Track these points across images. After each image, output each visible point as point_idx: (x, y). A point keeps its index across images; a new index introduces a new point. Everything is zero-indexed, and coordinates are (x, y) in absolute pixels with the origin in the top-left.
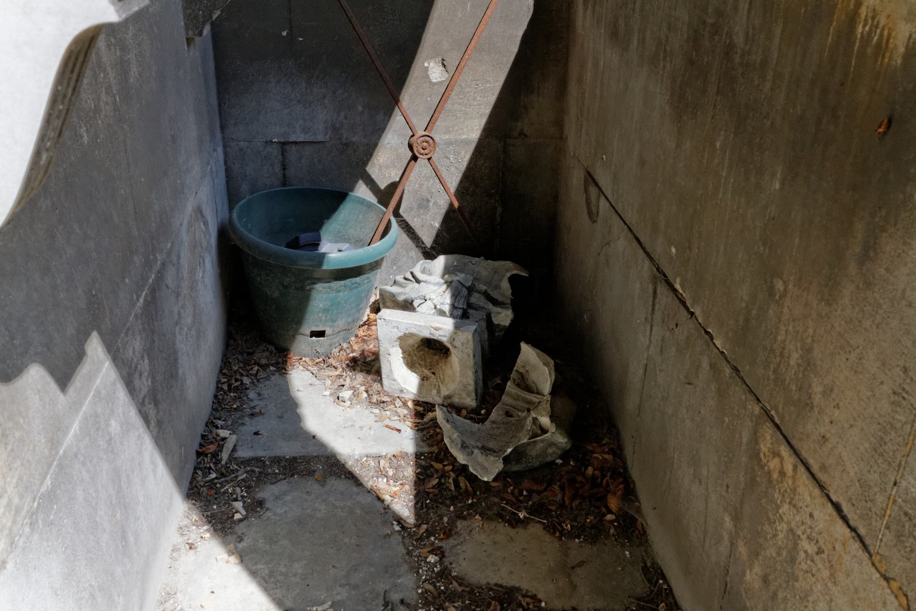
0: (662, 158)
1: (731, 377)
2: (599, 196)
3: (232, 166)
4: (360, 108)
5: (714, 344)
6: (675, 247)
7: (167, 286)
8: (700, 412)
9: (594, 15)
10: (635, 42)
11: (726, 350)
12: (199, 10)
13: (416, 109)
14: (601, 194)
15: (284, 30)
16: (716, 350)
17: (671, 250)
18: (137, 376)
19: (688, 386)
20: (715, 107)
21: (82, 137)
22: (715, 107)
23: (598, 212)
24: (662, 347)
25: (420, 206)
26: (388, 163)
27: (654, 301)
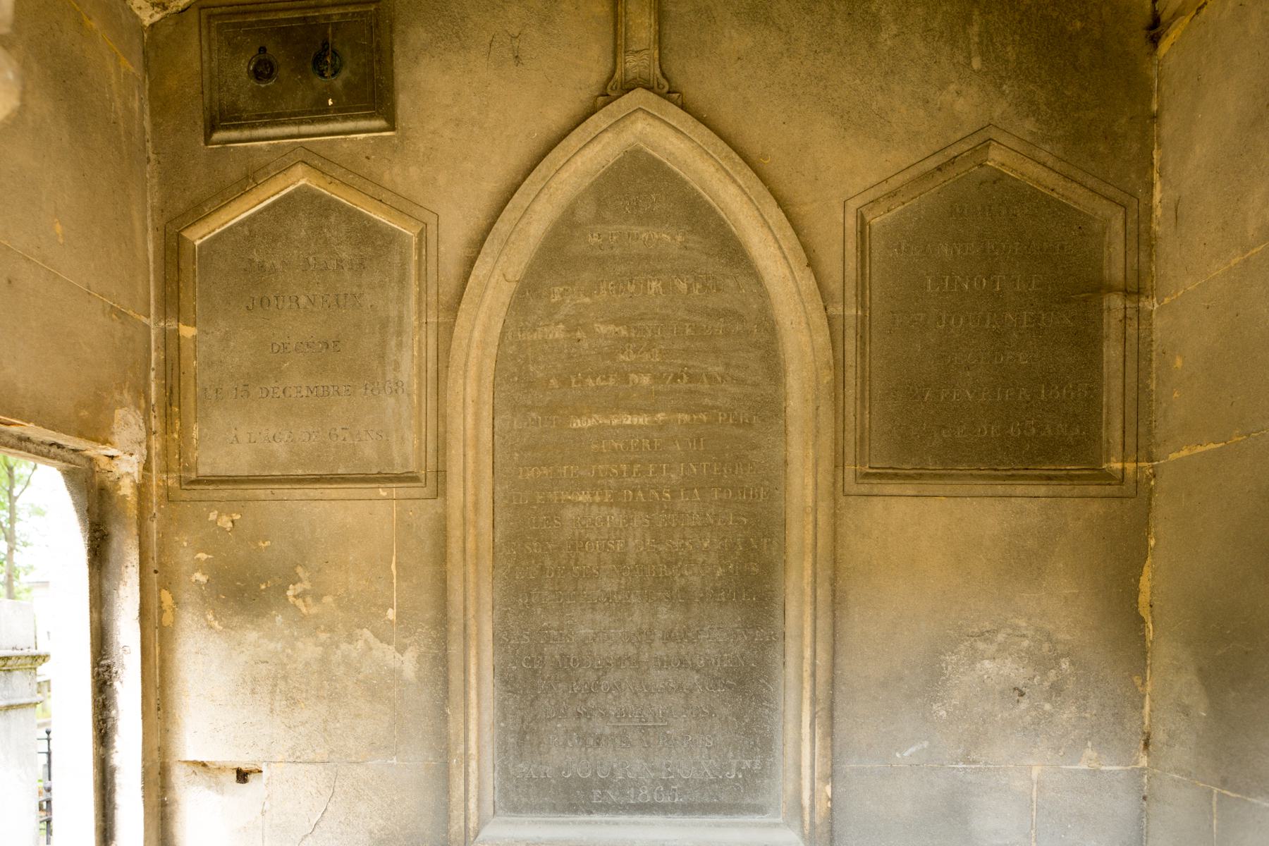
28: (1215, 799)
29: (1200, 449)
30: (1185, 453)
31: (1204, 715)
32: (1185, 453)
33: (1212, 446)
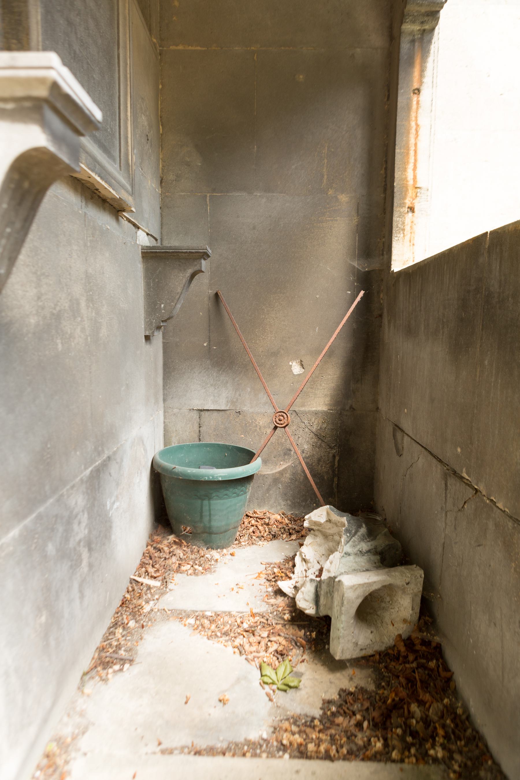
0: (446, 390)
1: (514, 528)
2: (403, 436)
3: (168, 424)
4: (249, 389)
5: (498, 507)
6: (460, 447)
7: (110, 474)
8: (490, 566)
9: (395, 327)
10: (423, 328)
11: (507, 508)
12: (153, 319)
13: (284, 390)
14: (405, 434)
15: (205, 343)
16: (499, 511)
17: (457, 451)
18: (76, 522)
19: (478, 548)
20: (481, 339)
21: (57, 345)
22: (481, 339)
23: (403, 448)
24: (455, 526)
25: (285, 454)
26: (265, 425)
27: (446, 493)
28: (208, 198)
29: (190, 48)
30: (181, 47)
31: (200, 164)
32: (181, 47)
33: (199, 48)
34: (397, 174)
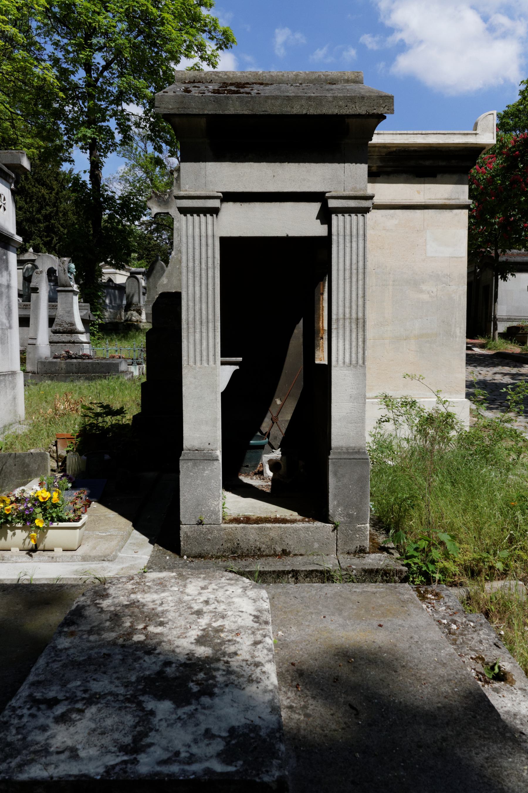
34: (316, 325)
